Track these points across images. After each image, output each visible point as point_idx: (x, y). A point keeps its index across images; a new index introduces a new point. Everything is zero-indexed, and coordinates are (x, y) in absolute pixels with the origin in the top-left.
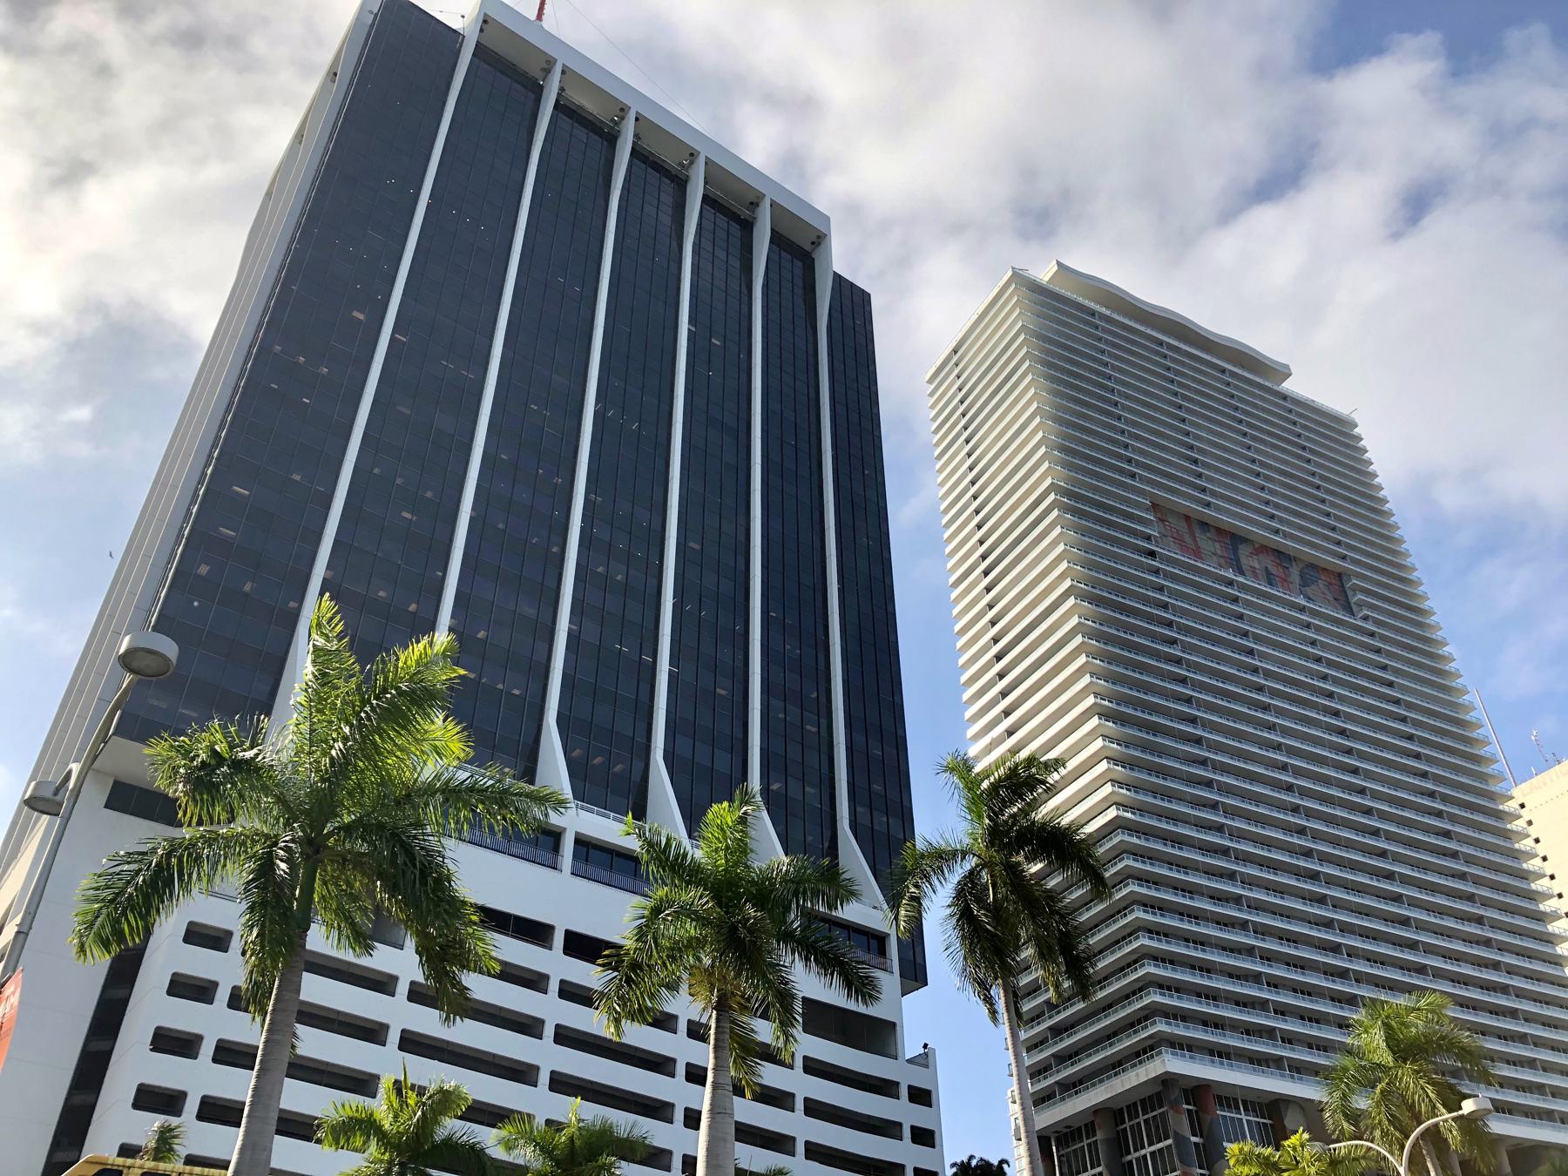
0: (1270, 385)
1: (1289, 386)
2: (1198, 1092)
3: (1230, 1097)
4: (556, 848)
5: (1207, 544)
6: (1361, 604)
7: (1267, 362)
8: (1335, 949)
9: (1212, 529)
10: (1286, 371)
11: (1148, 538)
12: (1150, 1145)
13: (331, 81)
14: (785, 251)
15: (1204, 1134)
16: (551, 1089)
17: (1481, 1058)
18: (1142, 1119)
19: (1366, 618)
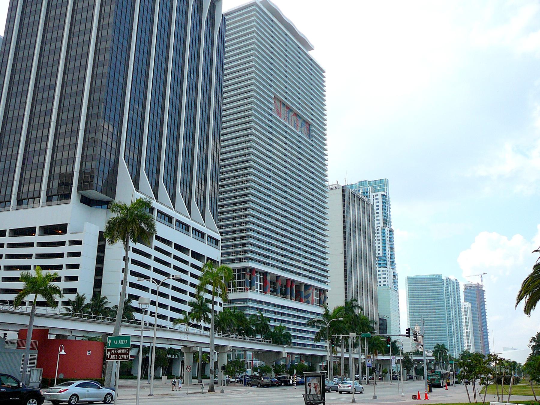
0: (305, 50)
1: (310, 53)
2: (252, 270)
3: (258, 271)
4: (189, 252)
5: (284, 110)
6: (313, 136)
7: (309, 44)
8: (299, 249)
9: (285, 106)
10: (313, 48)
11: (271, 109)
12: (237, 280)
13: (415, 340)
14: (468, 403)
15: (264, 289)
16: (152, 293)
17: (347, 302)
18: (236, 273)
19: (312, 140)
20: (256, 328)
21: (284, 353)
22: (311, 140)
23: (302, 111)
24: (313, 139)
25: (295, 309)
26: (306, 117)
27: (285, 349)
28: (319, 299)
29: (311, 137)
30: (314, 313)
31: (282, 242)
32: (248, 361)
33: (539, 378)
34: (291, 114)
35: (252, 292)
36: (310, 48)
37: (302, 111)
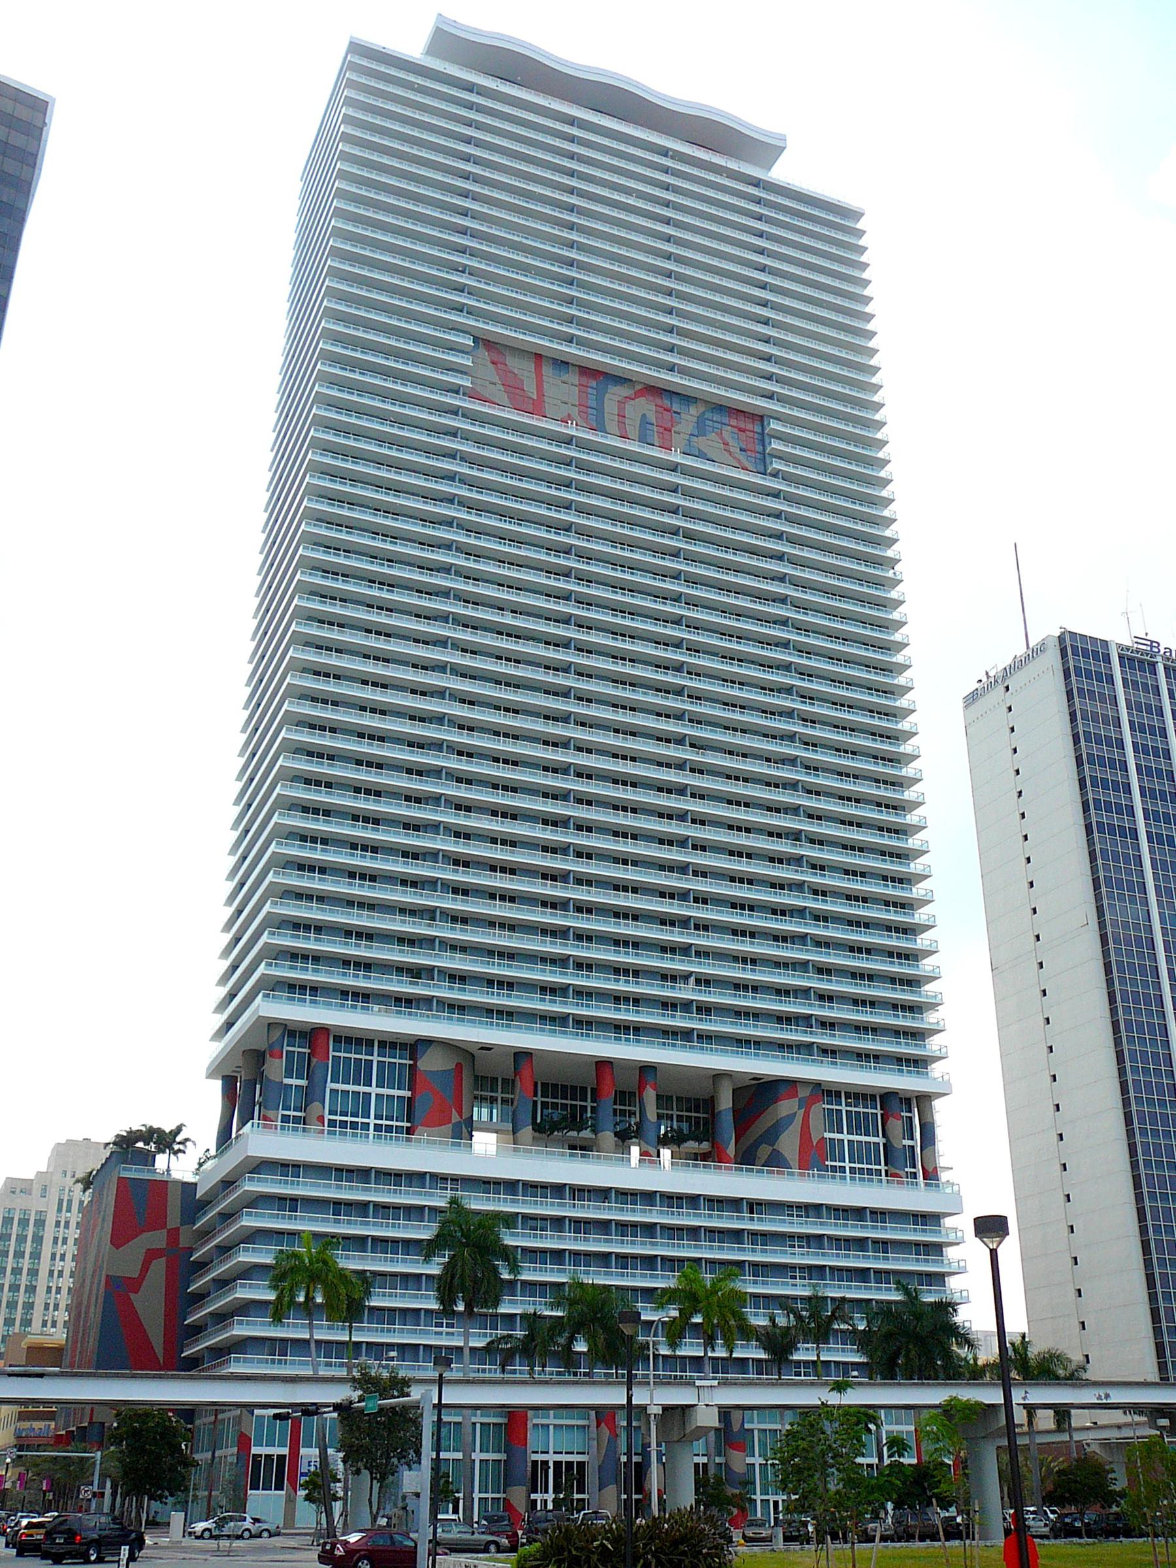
1: (782, 172)
7: (769, 141)
19: (775, 474)
20: (324, 1296)
21: (701, 1408)
22: (772, 475)
23: (684, 371)
24: (777, 465)
25: (558, 1190)
26: (704, 386)
27: (715, 1391)
28: (880, 1140)
29: (768, 459)
30: (818, 1207)
31: (780, 938)
32: (535, 1457)
33: (3, 1514)
34: (615, 393)
35: (606, 1158)
36: (769, 151)
37: (684, 371)
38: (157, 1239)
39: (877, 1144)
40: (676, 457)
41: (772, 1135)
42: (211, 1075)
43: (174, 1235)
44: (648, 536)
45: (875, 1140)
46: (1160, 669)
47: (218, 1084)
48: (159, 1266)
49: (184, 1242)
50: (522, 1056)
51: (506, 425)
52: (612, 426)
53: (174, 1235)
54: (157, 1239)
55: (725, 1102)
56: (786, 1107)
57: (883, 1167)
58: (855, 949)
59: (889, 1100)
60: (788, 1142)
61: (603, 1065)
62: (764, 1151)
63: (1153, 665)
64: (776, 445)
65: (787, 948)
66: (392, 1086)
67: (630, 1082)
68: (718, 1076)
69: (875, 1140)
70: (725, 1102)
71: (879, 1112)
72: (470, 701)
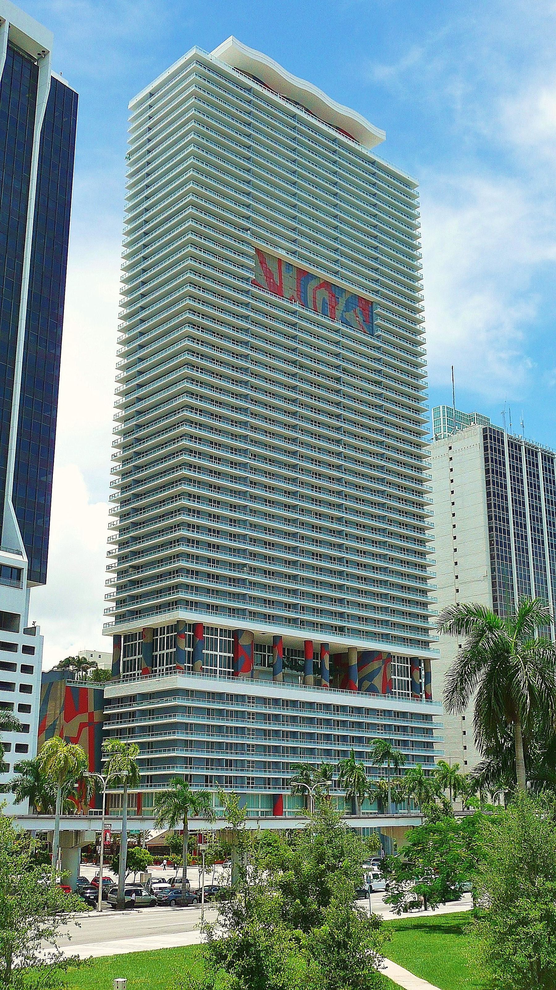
23: (343, 277)
28: (410, 679)
29: (375, 329)
38: (83, 718)
39: (408, 681)
40: (338, 325)
41: (370, 677)
42: (104, 633)
43: (91, 715)
44: (281, 351)
45: (406, 679)
46: (540, 455)
47: (111, 639)
48: (86, 730)
49: (96, 719)
50: (277, 639)
51: (354, 340)
52: (311, 304)
53: (91, 715)
54: (83, 718)
55: (354, 661)
56: (376, 665)
57: (410, 692)
58: (266, 544)
59: (415, 661)
60: (378, 681)
61: (308, 643)
62: (367, 684)
63: (520, 446)
64: (379, 321)
65: (211, 535)
66: (229, 652)
67: (318, 649)
68: (350, 649)
69: (406, 679)
70: (354, 661)
71: (409, 666)
72: (272, 461)
